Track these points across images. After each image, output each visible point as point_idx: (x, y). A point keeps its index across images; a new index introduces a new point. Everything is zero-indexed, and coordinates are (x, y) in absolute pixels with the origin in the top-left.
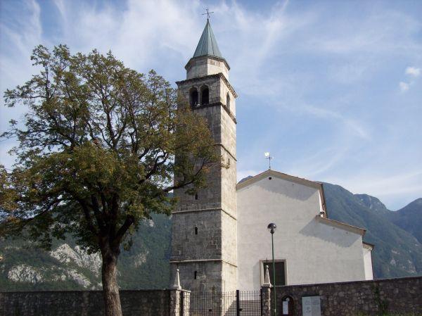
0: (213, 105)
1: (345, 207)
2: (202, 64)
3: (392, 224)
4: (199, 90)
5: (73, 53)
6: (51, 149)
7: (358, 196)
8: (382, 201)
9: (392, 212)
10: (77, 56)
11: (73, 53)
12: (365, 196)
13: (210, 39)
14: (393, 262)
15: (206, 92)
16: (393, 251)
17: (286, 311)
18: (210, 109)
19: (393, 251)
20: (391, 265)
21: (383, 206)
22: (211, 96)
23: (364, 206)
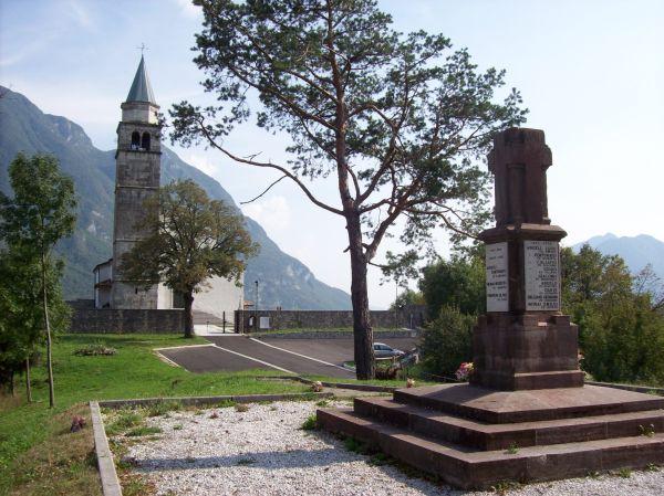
0: (153, 153)
1: (27, 133)
2: (143, 109)
3: (98, 171)
4: (141, 135)
5: (471, 61)
6: (177, 143)
7: (52, 118)
8: (87, 131)
9: (99, 152)
10: (480, 71)
11: (471, 61)
12: (61, 120)
13: (140, 89)
14: (92, 228)
15: (147, 138)
16: (94, 212)
17: (251, 323)
18: (151, 155)
19: (94, 212)
20: (89, 233)
21: (88, 140)
22: (153, 143)
23: (58, 135)
